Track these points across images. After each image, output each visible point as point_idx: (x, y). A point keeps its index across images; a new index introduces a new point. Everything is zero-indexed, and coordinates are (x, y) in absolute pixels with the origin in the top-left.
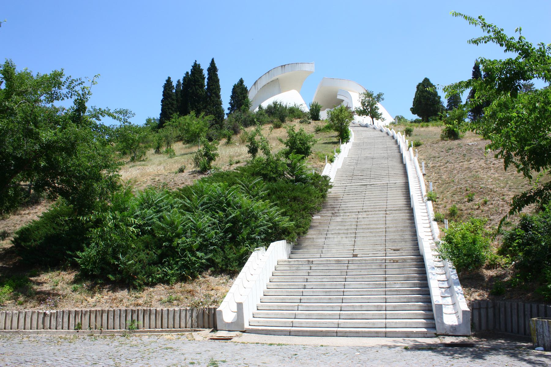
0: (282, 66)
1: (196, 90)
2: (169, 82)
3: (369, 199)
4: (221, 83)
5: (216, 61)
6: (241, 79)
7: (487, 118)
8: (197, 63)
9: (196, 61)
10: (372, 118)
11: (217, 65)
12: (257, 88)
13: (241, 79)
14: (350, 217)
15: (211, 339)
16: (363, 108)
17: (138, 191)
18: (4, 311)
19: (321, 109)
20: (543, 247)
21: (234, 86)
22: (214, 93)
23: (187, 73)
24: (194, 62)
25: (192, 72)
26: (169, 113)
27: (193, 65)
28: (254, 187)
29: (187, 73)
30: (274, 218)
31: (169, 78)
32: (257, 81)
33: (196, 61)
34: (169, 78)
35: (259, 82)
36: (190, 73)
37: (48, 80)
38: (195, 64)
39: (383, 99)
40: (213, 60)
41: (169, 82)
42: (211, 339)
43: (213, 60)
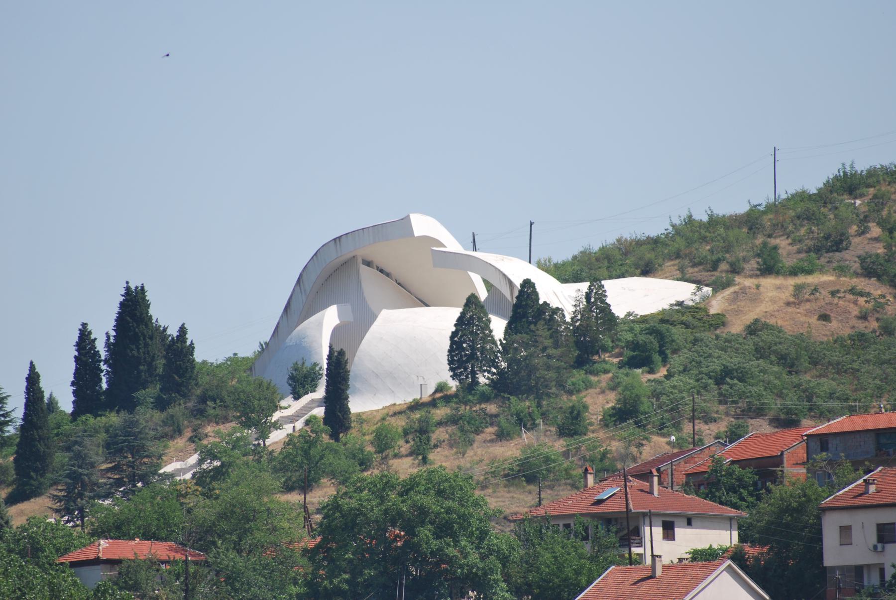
0: (335, 239)
2: (84, 340)
12: (305, 290)
31: (84, 325)
33: (127, 282)
34: (84, 325)
35: (304, 275)
38: (128, 289)
43: (31, 363)
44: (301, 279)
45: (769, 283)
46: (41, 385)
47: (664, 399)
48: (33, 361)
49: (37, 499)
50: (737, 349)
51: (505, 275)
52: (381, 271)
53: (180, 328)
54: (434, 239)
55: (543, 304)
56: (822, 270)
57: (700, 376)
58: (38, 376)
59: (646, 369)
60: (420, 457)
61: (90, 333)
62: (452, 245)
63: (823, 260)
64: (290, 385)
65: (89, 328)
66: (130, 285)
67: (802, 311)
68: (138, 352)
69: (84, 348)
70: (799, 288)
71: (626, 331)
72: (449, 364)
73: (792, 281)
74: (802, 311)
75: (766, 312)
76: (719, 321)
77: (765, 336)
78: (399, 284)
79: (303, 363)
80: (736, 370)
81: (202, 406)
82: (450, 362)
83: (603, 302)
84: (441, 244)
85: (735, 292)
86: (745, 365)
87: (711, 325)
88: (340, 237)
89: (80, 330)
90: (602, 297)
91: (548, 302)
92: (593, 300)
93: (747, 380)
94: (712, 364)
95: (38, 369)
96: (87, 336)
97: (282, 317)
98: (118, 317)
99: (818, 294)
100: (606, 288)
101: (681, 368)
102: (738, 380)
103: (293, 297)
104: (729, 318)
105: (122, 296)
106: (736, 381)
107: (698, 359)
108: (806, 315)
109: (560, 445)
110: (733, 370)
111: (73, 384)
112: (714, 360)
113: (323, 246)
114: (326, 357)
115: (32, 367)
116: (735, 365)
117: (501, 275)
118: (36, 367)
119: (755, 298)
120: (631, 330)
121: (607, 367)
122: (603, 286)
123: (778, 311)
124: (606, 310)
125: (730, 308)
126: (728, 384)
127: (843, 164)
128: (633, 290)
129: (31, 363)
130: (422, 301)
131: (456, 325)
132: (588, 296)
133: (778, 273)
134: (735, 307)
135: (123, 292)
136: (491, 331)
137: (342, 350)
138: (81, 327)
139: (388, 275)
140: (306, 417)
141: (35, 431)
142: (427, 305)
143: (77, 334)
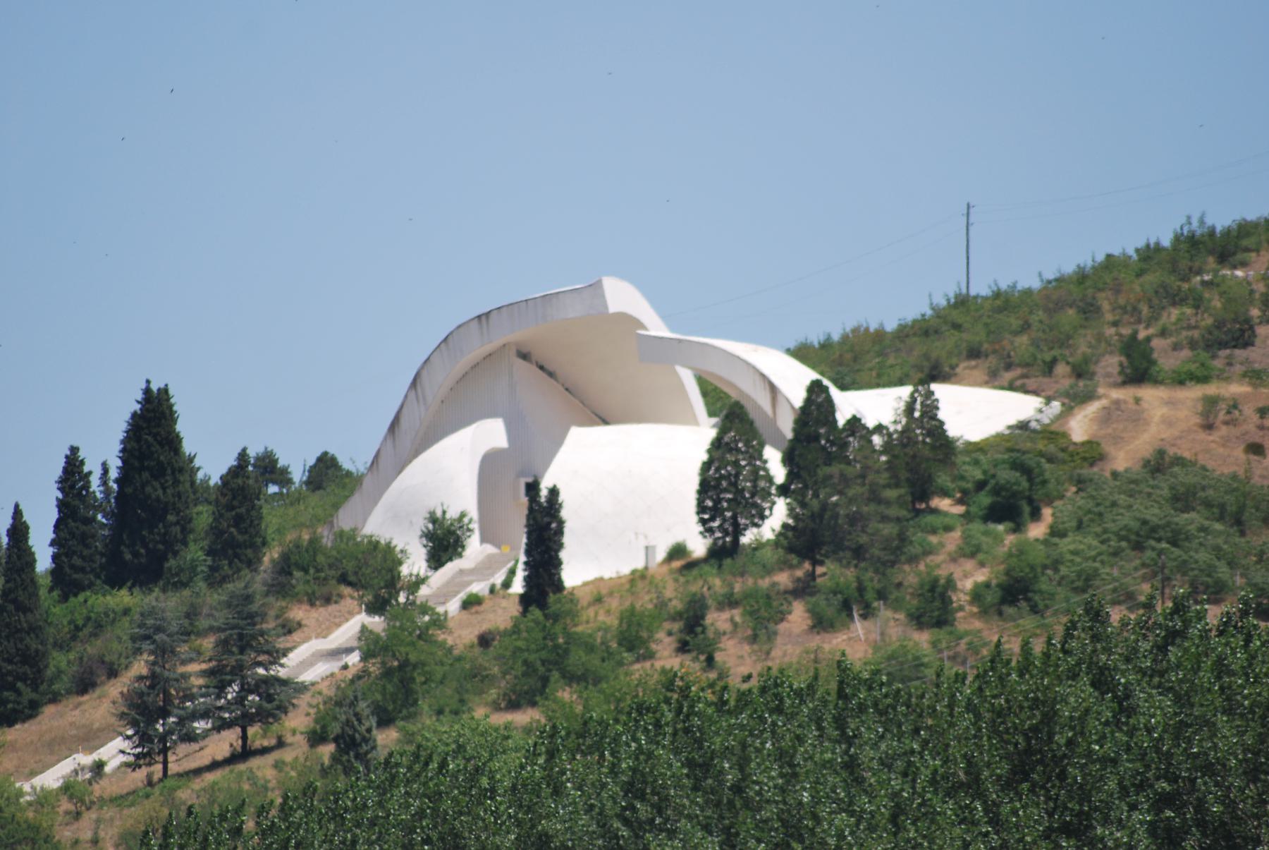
0: (479, 317)
1: (143, 486)
2: (73, 470)
7: (1116, 615)
9: (148, 382)
12: (424, 398)
17: (349, 604)
18: (499, 741)
24: (144, 386)
26: (72, 567)
29: (57, 498)
30: (823, 721)
31: (74, 450)
32: (451, 333)
33: (148, 382)
34: (74, 450)
35: (424, 374)
38: (147, 391)
41: (73, 470)
43: (17, 506)
44: (418, 381)
45: (1150, 395)
46: (31, 542)
47: (1064, 570)
48: (20, 503)
49: (26, 725)
50: (1149, 495)
51: (763, 376)
52: (542, 368)
53: (239, 454)
54: (635, 318)
55: (62, 493)
56: (1223, 377)
57: (1105, 536)
58: (27, 528)
59: (1010, 525)
60: (702, 658)
61: (82, 463)
62: (656, 328)
63: (1218, 364)
64: (425, 546)
65: (81, 454)
67: (1218, 439)
68: (165, 492)
69: (72, 487)
70: (1211, 403)
71: (969, 464)
72: (698, 513)
73: (1194, 393)
74: (1218, 439)
75: (1162, 440)
76: (1092, 453)
77: (1183, 477)
78: (567, 389)
79: (444, 512)
80: (1163, 527)
81: (283, 579)
82: (701, 509)
83: (934, 418)
84: (643, 327)
85: (1104, 408)
86: (1176, 520)
87: (1084, 459)
88: (488, 314)
89: (67, 457)
90: (931, 409)
91: (858, 416)
92: (917, 414)
93: (1180, 543)
94: (1120, 517)
95: (27, 517)
96: (78, 467)
97: (385, 439)
98: (126, 438)
99: (1237, 412)
100: (937, 395)
101: (1074, 524)
102: (1168, 542)
103: (405, 410)
104: (1107, 448)
105: (138, 402)
106: (1164, 545)
107: (1096, 510)
108: (1224, 446)
109: (922, 639)
110: (1158, 526)
111: (52, 544)
112: (1122, 511)
113: (459, 327)
114: (50, 535)
115: (17, 513)
116: (1160, 519)
117: (757, 377)
118: (24, 514)
119: (1137, 419)
120: (976, 462)
121: (947, 520)
122: (932, 393)
123: (1180, 438)
124: (937, 430)
125: (1103, 432)
126: (1153, 549)
127: (1189, 218)
128: (351, 459)
129: (17, 506)
130: (600, 418)
131: (709, 451)
132: (910, 409)
133: (1157, 382)
134: (1110, 431)
135: (140, 396)
136: (765, 462)
137: (555, 486)
138: (68, 453)
139: (551, 374)
140: (462, 596)
141: (22, 616)
142: (605, 422)
143: (61, 463)
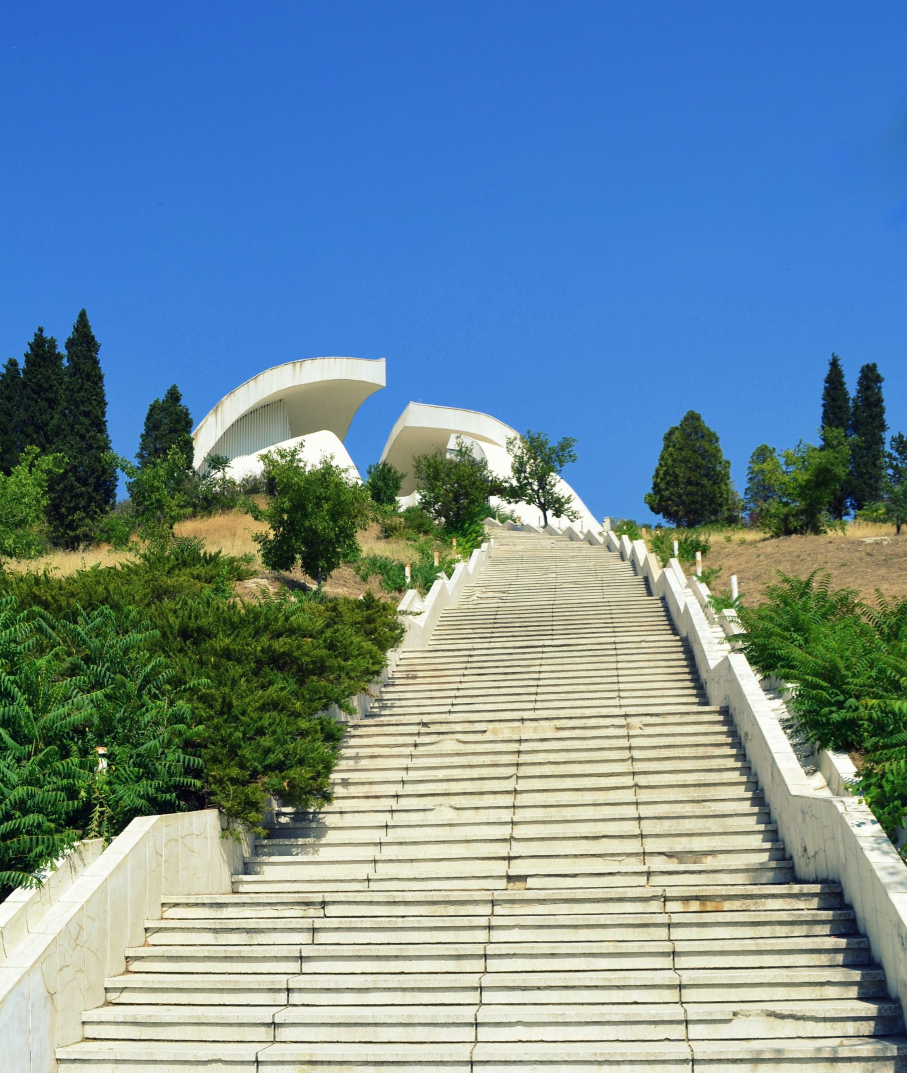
3: (496, 621)
4: (111, 389)
5: (89, 316)
6: (174, 388)
8: (47, 335)
9: (41, 330)
10: (543, 507)
11: (97, 331)
13: (174, 388)
14: (126, 775)
15: (418, 614)
16: (518, 480)
19: (568, 466)
20: (862, 735)
21: (153, 408)
22: (86, 414)
23: (13, 364)
25: (28, 361)
27: (32, 340)
28: (856, 684)
29: (13, 364)
33: (41, 330)
36: (22, 365)
37: (108, 541)
39: (888, 428)
40: (83, 315)
42: (421, 613)
43: (83, 315)
66: (45, 335)
